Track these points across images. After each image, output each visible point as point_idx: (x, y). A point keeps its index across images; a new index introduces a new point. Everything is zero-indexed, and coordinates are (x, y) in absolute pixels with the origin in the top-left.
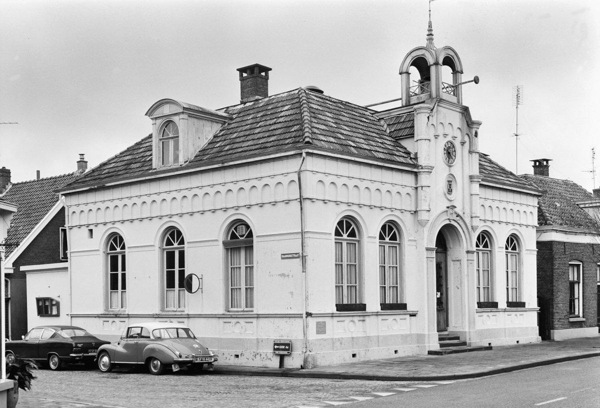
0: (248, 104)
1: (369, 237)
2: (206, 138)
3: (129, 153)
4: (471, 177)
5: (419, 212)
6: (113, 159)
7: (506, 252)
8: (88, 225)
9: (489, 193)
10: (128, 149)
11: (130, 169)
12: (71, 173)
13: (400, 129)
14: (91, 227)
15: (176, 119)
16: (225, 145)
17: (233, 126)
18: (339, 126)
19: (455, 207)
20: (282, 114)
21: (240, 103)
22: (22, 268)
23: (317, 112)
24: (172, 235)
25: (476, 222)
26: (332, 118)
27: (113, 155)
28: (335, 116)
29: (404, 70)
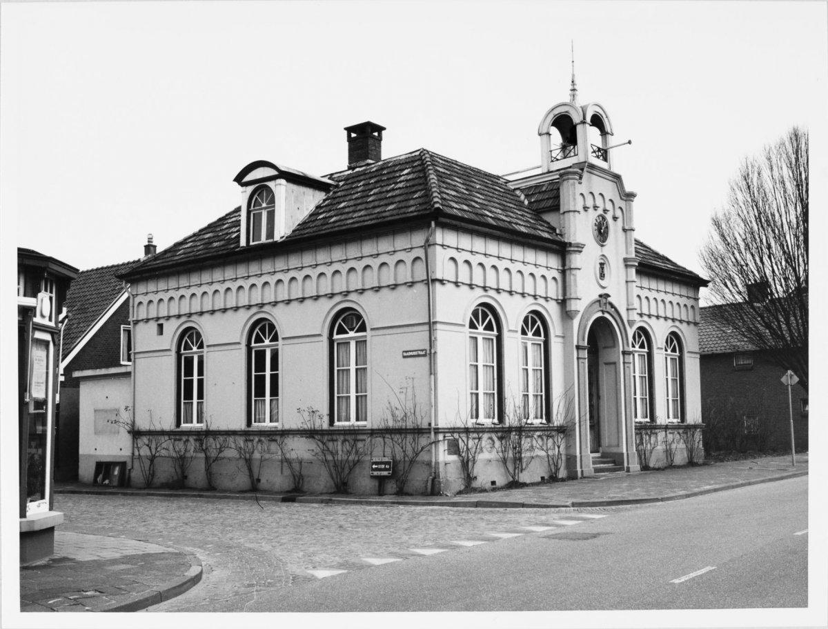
0: (357, 170)
1: (510, 331)
2: (307, 209)
3: (210, 230)
4: (625, 260)
5: (568, 302)
6: (190, 237)
7: (666, 354)
8: (158, 319)
9: (645, 282)
10: (210, 226)
11: (213, 251)
12: (136, 259)
13: (541, 200)
14: (160, 322)
15: (271, 184)
16: (332, 217)
17: (339, 194)
18: (471, 193)
19: (610, 296)
20: (402, 178)
21: (347, 169)
22: (76, 374)
23: (443, 175)
24: (263, 330)
25: (634, 316)
26: (463, 184)
27: (190, 233)
28: (465, 182)
29: (545, 131)
